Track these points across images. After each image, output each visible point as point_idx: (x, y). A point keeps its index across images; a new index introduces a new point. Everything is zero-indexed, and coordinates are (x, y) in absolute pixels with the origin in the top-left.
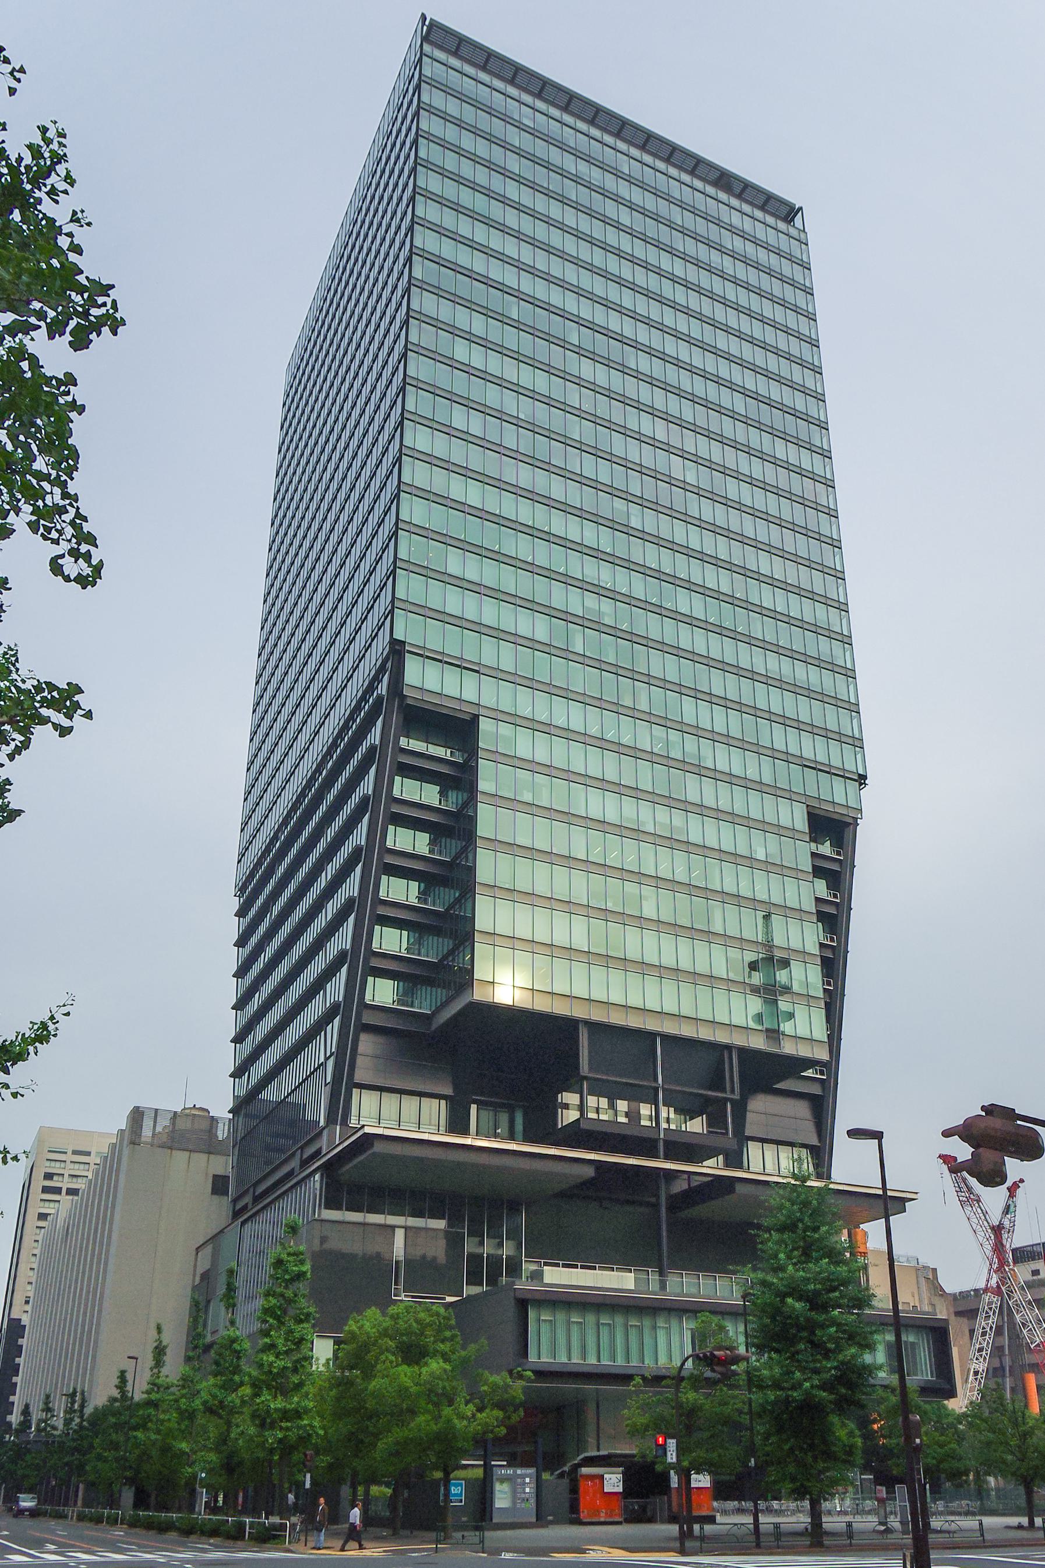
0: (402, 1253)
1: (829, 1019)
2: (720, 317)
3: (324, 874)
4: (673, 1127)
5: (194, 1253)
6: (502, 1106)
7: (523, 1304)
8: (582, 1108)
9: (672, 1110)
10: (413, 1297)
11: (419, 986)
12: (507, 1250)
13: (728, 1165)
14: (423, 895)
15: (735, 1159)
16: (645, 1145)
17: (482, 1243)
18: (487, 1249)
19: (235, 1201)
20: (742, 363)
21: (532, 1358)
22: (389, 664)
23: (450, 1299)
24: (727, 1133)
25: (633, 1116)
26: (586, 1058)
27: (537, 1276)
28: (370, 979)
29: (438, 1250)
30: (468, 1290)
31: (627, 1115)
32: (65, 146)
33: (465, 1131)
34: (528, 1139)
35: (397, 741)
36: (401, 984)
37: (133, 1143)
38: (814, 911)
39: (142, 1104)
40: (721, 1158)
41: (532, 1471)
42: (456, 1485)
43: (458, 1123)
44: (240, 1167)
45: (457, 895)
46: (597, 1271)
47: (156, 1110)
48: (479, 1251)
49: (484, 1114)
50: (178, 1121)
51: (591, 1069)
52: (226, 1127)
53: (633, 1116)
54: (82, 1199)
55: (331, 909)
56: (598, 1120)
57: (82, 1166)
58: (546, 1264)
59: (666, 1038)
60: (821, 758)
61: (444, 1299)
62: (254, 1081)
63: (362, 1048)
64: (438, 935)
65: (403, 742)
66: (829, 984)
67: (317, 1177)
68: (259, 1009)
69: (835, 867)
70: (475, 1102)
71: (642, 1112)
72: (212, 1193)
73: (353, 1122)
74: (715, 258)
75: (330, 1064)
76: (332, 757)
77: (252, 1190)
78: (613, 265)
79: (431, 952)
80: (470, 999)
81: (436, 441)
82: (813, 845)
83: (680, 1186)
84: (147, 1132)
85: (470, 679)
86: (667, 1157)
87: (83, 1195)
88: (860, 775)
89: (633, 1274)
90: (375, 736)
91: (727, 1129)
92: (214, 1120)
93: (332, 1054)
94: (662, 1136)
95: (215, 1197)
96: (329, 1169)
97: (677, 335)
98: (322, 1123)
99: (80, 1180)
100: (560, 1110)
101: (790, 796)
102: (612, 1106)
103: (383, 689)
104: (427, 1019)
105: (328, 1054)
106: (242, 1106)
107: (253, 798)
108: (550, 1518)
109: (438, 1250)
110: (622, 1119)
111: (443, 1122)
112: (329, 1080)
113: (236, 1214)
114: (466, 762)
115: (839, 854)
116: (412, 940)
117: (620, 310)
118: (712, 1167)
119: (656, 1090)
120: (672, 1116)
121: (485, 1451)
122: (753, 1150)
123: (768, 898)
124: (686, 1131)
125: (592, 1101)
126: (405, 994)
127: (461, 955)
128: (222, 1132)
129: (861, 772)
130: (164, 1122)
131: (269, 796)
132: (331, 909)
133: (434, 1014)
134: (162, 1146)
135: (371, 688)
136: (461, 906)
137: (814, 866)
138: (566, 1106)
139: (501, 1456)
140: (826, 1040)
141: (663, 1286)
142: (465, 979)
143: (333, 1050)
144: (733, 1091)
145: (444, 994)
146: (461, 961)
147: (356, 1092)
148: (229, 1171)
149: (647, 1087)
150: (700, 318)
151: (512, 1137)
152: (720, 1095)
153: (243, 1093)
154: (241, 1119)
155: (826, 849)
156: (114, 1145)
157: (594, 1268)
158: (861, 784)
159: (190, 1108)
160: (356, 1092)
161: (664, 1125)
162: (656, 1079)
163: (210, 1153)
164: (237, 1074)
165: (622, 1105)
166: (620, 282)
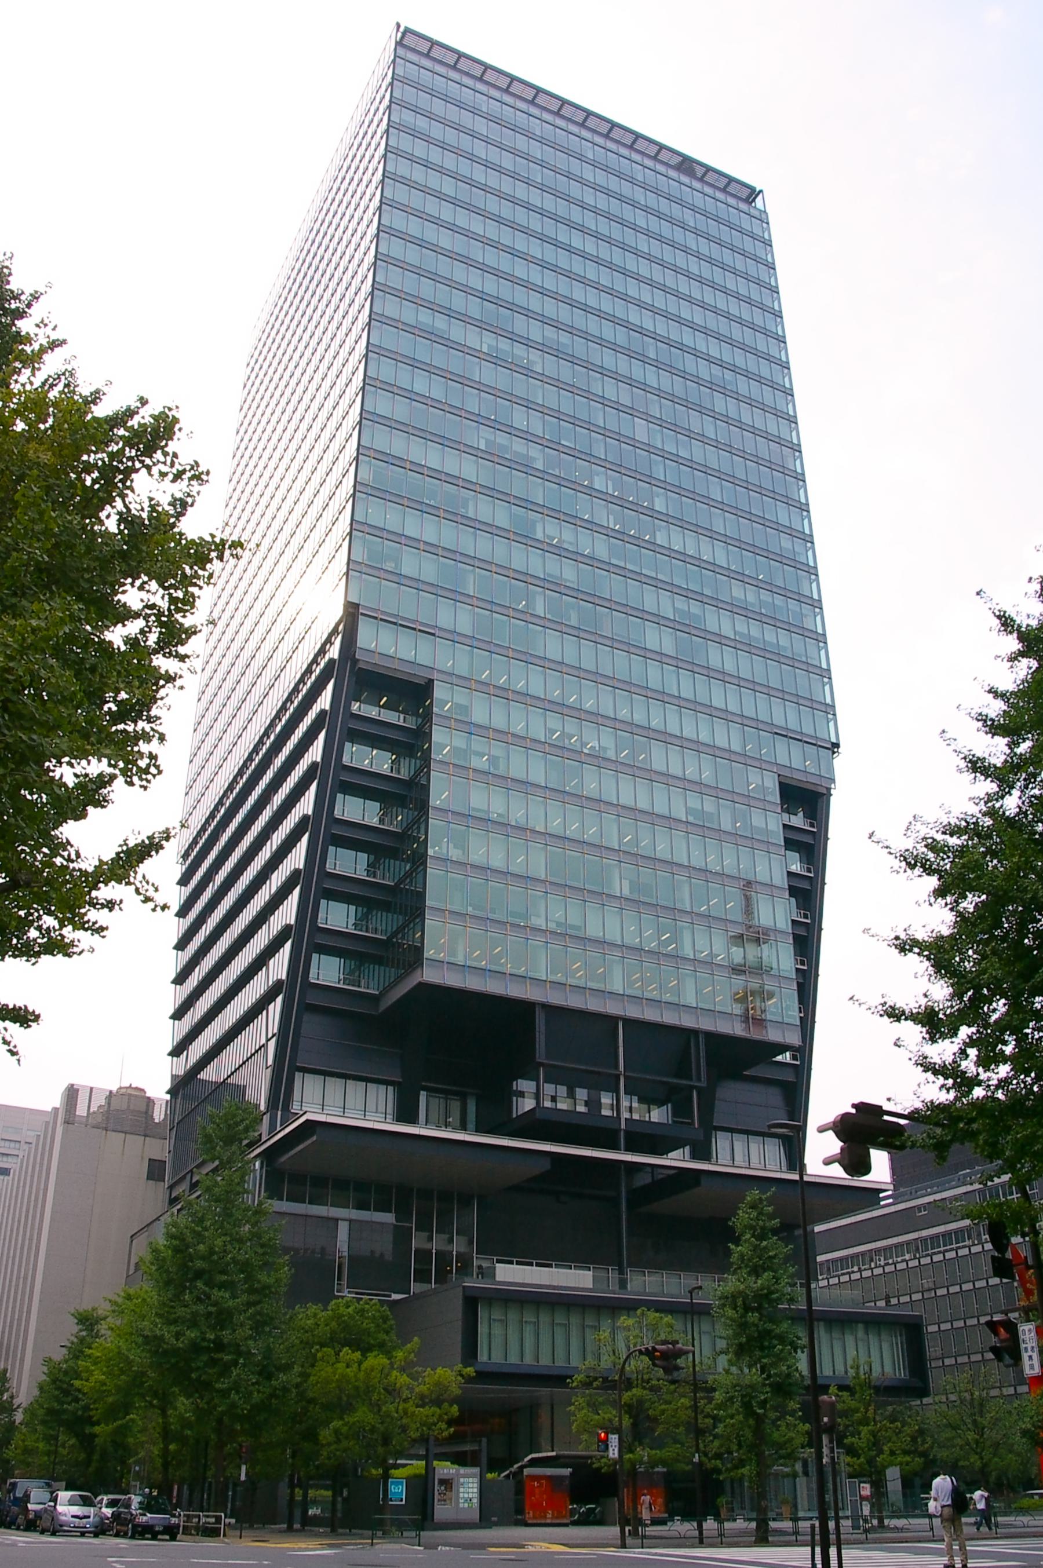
0: (346, 1248)
1: (801, 1001)
2: (684, 289)
3: (269, 843)
4: (636, 1117)
5: (129, 1241)
6: (455, 1093)
7: (472, 1302)
8: (537, 1096)
9: (635, 1098)
10: (357, 1293)
11: (366, 965)
12: (457, 1246)
13: (695, 1156)
14: (372, 868)
15: (702, 1151)
16: (606, 1137)
17: (430, 1239)
18: (436, 1244)
19: (171, 1188)
20: (706, 332)
21: (483, 1357)
22: (341, 628)
23: (396, 1297)
24: (693, 1123)
25: (593, 1104)
26: (543, 1044)
27: (489, 1274)
28: (315, 956)
29: (384, 1246)
30: (414, 1287)
31: (587, 1104)
32: (144, 902)
33: (413, 1120)
34: (479, 1130)
35: (348, 706)
36: (348, 962)
37: (67, 1122)
38: (787, 887)
39: (78, 1081)
40: (687, 1149)
41: (476, 1470)
42: (397, 1484)
43: (406, 1112)
44: (177, 1153)
45: (408, 868)
46: (554, 1269)
47: (91, 1089)
48: (427, 1246)
49: (434, 1102)
50: (113, 1099)
51: (547, 1058)
52: (163, 1109)
53: (593, 1104)
54: (13, 1179)
55: (277, 879)
56: (556, 1109)
57: (12, 1145)
58: (499, 1261)
59: (629, 1022)
60: (793, 724)
61: (390, 1296)
62: (262, 974)
63: (305, 1028)
64: (388, 911)
65: (355, 707)
66: (802, 963)
67: (257, 1164)
68: (198, 987)
69: (808, 839)
70: (424, 1088)
71: (603, 1100)
72: (148, 1178)
73: (295, 1107)
74: (676, 211)
75: (272, 1044)
76: (280, 720)
77: (188, 1177)
78: (578, 293)
79: (381, 926)
80: (420, 980)
81: (408, 520)
82: (785, 816)
83: (642, 1180)
84: (81, 1110)
85: (424, 642)
86: (630, 1149)
87: (14, 1175)
88: (833, 744)
89: (591, 1273)
90: (324, 701)
91: (693, 1120)
92: (150, 1102)
93: (274, 1035)
94: (623, 1126)
95: (151, 1182)
96: (270, 1156)
97: (640, 305)
98: (263, 1108)
99: (10, 1159)
100: (514, 1098)
101: (760, 764)
102: (571, 1095)
103: (334, 652)
104: (375, 999)
105: (270, 1035)
106: (182, 1086)
107: (198, 761)
108: (494, 1519)
109: (384, 1246)
110: (581, 1108)
111: (390, 1110)
112: (270, 1062)
113: (173, 1201)
114: (420, 728)
115: (812, 825)
116: (359, 915)
117: (583, 281)
118: (678, 1159)
119: (618, 1077)
120: (635, 1105)
121: (427, 1450)
122: (721, 1143)
123: (720, 666)
124: (650, 1122)
125: (549, 1089)
126: (351, 972)
127: (411, 932)
128: (159, 1115)
129: (834, 740)
130: (99, 1101)
131: (215, 760)
132: (277, 879)
133: (382, 995)
134: (96, 1127)
135: (322, 651)
136: (411, 881)
137: (786, 840)
138: (522, 1094)
139: (442, 1457)
140: (798, 1023)
141: (623, 1284)
142: (415, 957)
143: (276, 1031)
144: (699, 1079)
145: (393, 975)
146: (411, 939)
147: (298, 1076)
148: (166, 1156)
149: (610, 1075)
150: (664, 289)
151: (463, 1127)
152: (684, 1082)
153: (181, 1072)
154: (179, 1101)
155: (798, 820)
156: (47, 1123)
157: (550, 1266)
158: (834, 753)
159: (126, 1088)
160: (298, 1076)
161: (625, 1115)
162: (617, 1067)
163: (145, 1136)
164: (177, 1052)
165: (582, 1094)
166: (585, 309)
